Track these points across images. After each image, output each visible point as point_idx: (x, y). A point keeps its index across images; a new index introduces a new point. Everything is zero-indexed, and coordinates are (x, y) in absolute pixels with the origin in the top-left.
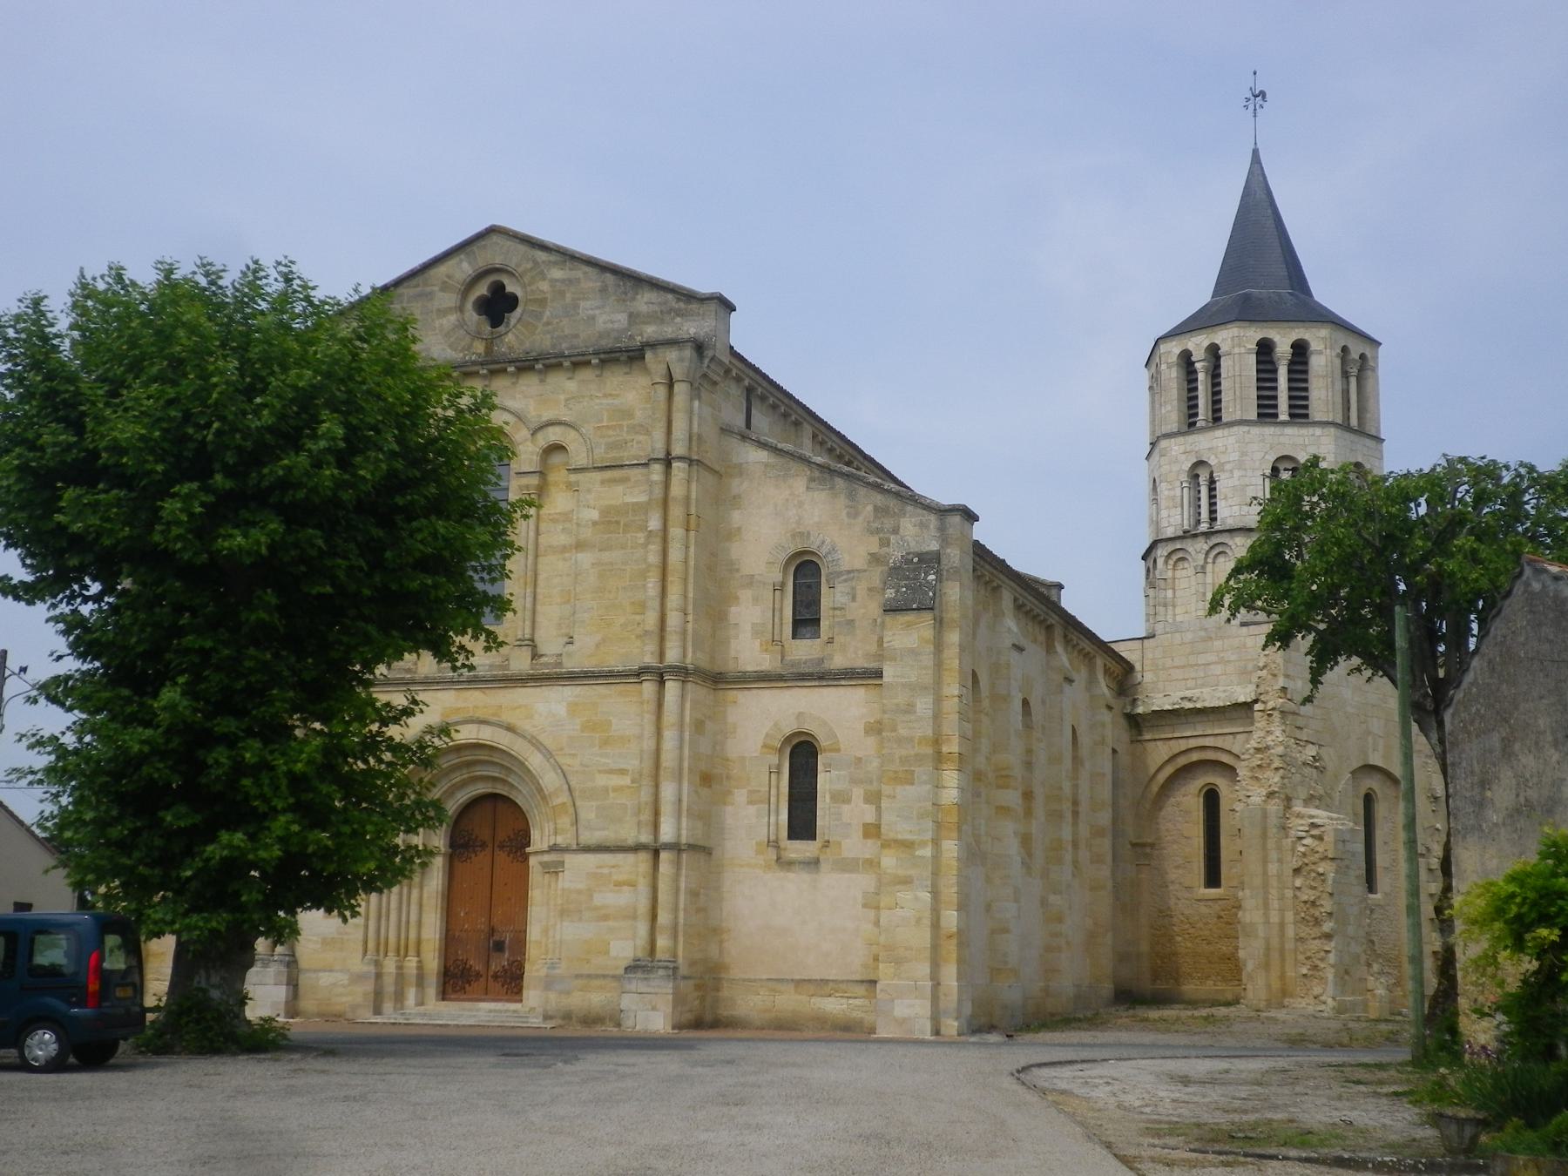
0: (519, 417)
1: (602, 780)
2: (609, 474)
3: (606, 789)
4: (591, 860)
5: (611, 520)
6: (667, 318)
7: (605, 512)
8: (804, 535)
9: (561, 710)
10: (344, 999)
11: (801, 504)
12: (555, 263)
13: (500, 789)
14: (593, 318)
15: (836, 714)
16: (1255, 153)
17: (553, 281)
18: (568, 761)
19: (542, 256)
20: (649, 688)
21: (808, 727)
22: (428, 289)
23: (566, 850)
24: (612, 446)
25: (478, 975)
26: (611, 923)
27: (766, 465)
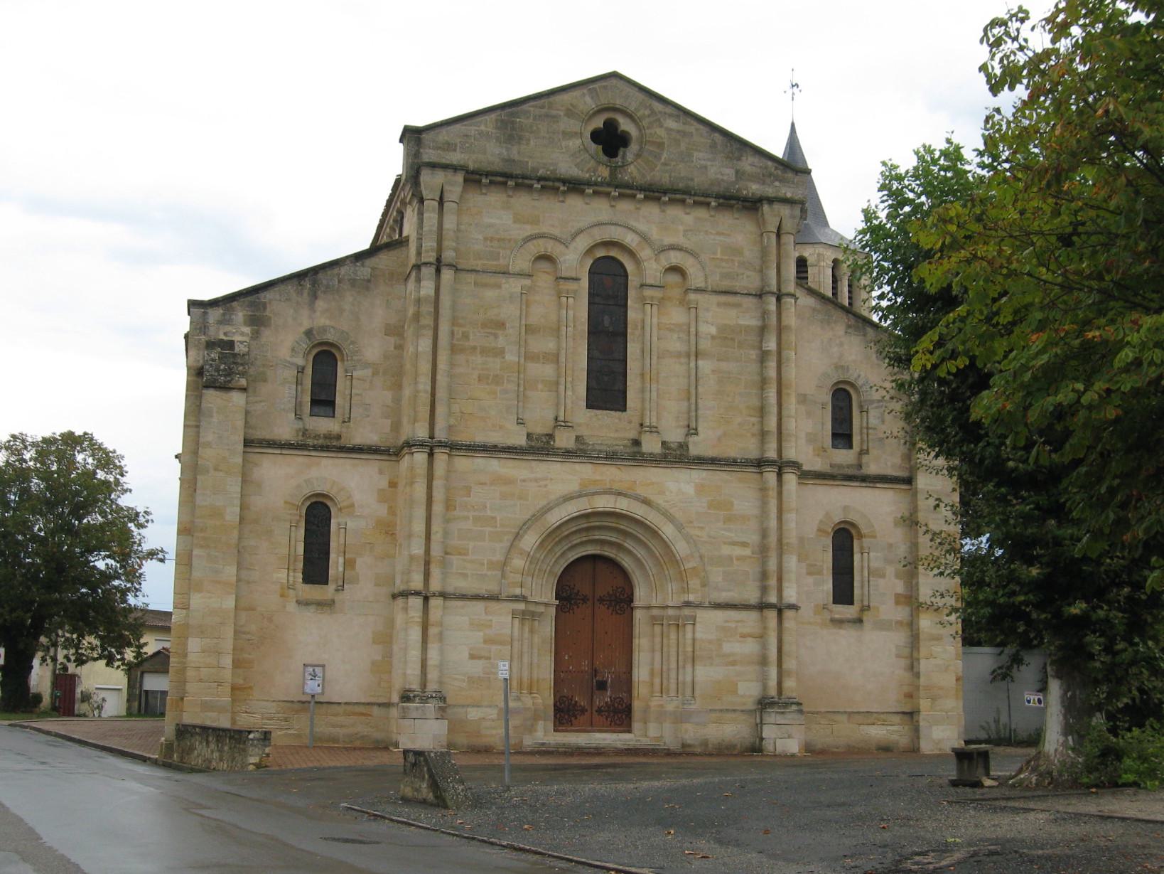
0: (645, 238)
1: (726, 550)
2: (723, 298)
3: (730, 558)
4: (720, 615)
5: (726, 335)
6: (768, 180)
7: (723, 329)
8: (844, 368)
9: (690, 490)
10: (494, 732)
11: (841, 344)
12: (670, 115)
13: (609, 552)
14: (706, 167)
15: (876, 509)
16: (793, 125)
17: (669, 130)
18: (697, 532)
19: (658, 106)
20: (771, 477)
21: (852, 517)
22: (554, 112)
23: (699, 606)
24: (725, 276)
25: (583, 711)
26: (738, 668)
27: (814, 309)
